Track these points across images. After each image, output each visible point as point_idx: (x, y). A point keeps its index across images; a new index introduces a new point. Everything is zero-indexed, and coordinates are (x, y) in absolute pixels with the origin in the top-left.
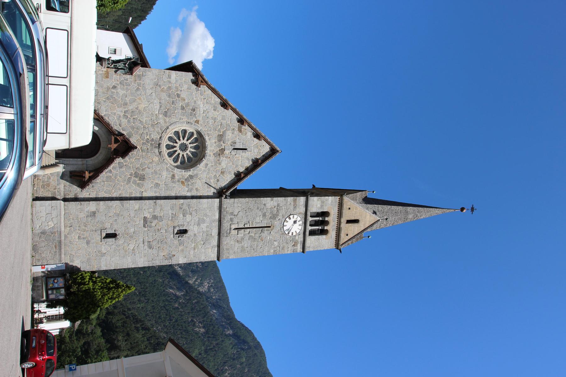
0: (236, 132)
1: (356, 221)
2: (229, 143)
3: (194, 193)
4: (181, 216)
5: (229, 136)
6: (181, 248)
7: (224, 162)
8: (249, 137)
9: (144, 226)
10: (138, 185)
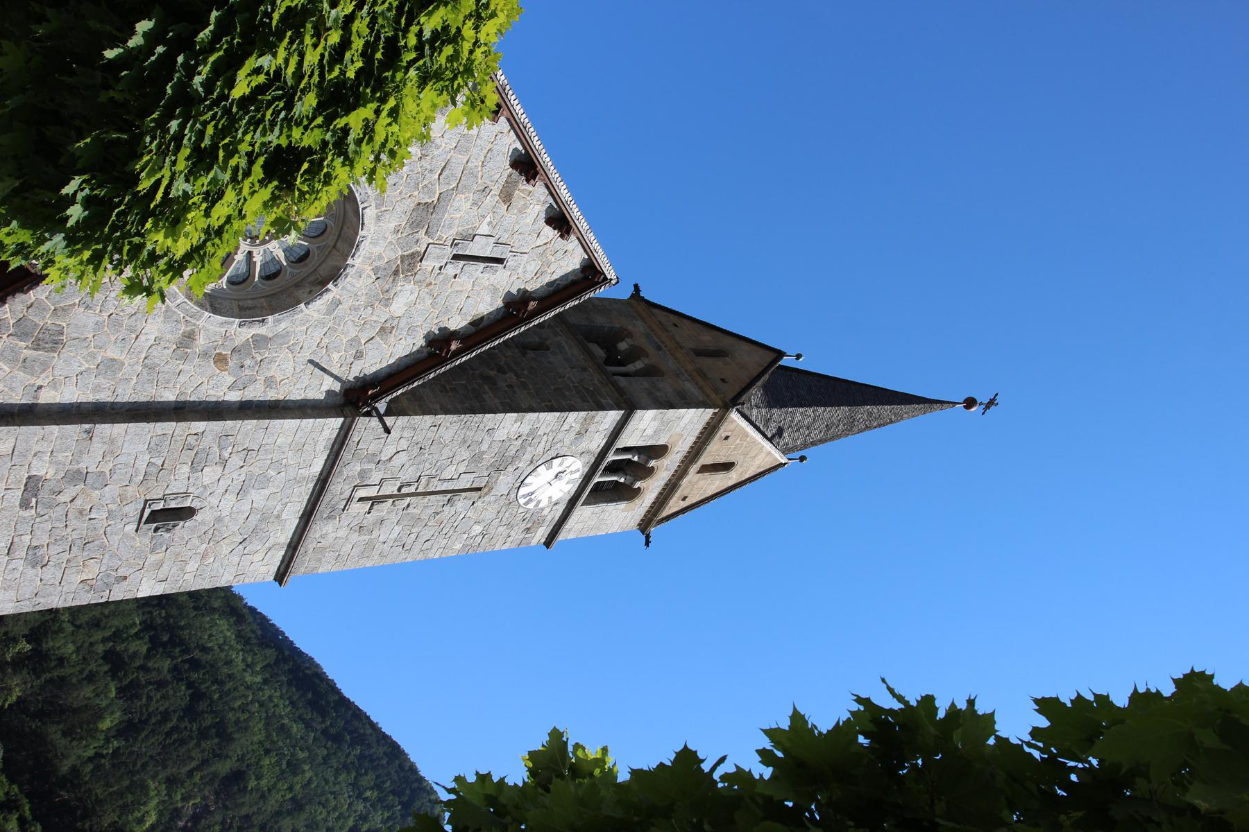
0: (491, 200)
1: (727, 466)
2: (449, 234)
3: (255, 393)
4: (186, 469)
5: (460, 213)
6: (153, 558)
7: (406, 295)
8: (529, 220)
9: (25, 504)
10: (25, 364)
